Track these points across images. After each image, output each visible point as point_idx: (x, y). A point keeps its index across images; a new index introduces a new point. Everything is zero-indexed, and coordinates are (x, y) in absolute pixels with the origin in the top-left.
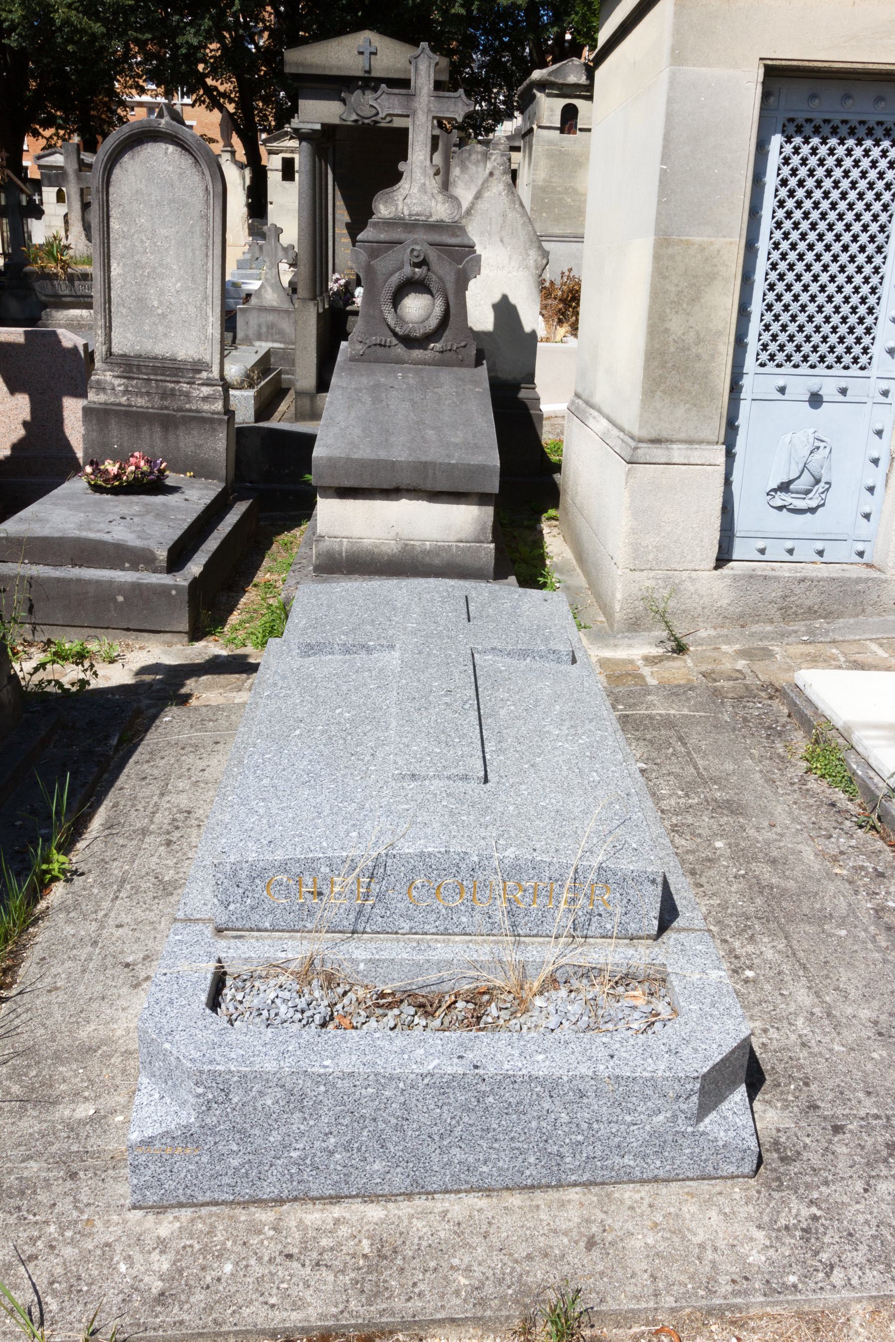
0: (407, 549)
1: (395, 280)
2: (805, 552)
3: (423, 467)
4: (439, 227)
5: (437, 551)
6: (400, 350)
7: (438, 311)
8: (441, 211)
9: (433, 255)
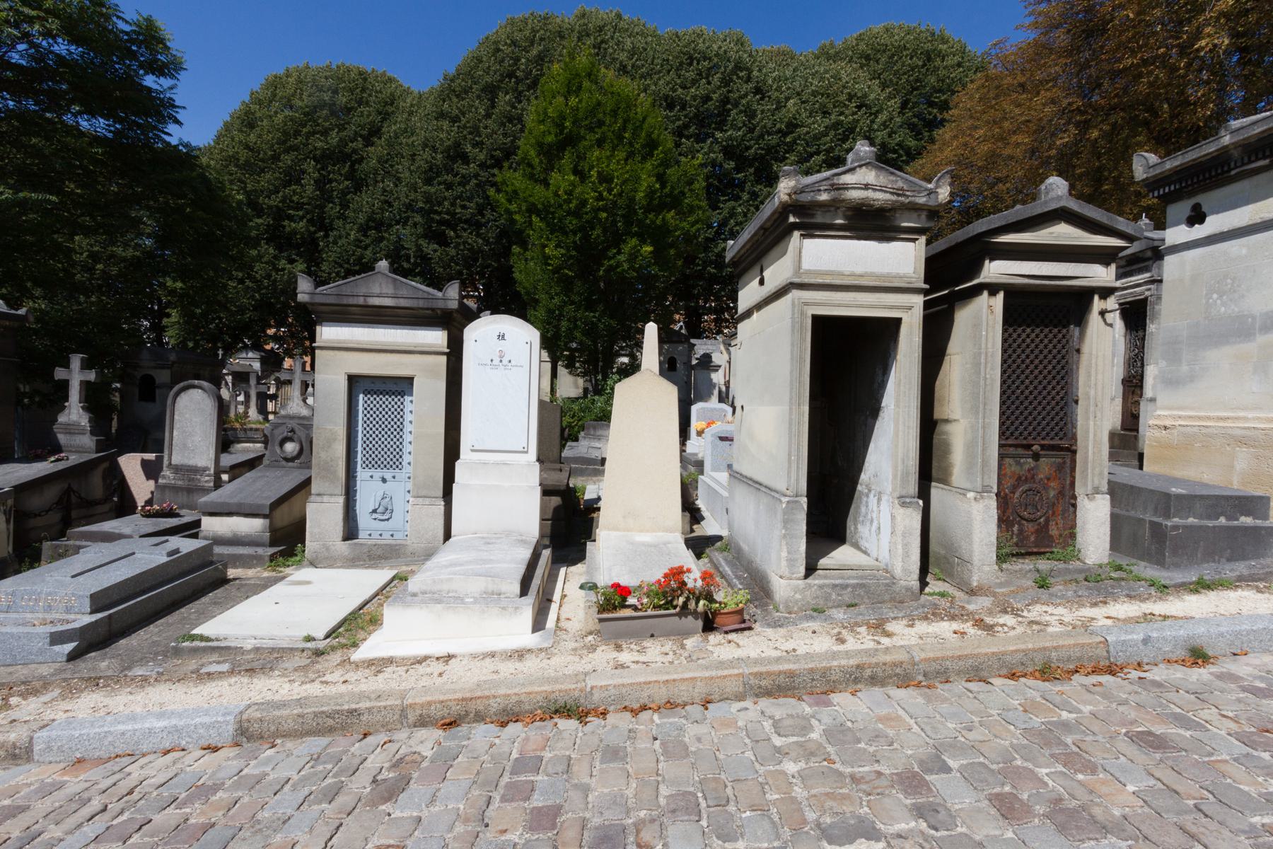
0: (235, 535)
1: (280, 437)
2: (386, 535)
3: (240, 505)
4: (304, 418)
5: (247, 536)
6: (284, 463)
7: (298, 448)
8: (305, 412)
9: (297, 428)
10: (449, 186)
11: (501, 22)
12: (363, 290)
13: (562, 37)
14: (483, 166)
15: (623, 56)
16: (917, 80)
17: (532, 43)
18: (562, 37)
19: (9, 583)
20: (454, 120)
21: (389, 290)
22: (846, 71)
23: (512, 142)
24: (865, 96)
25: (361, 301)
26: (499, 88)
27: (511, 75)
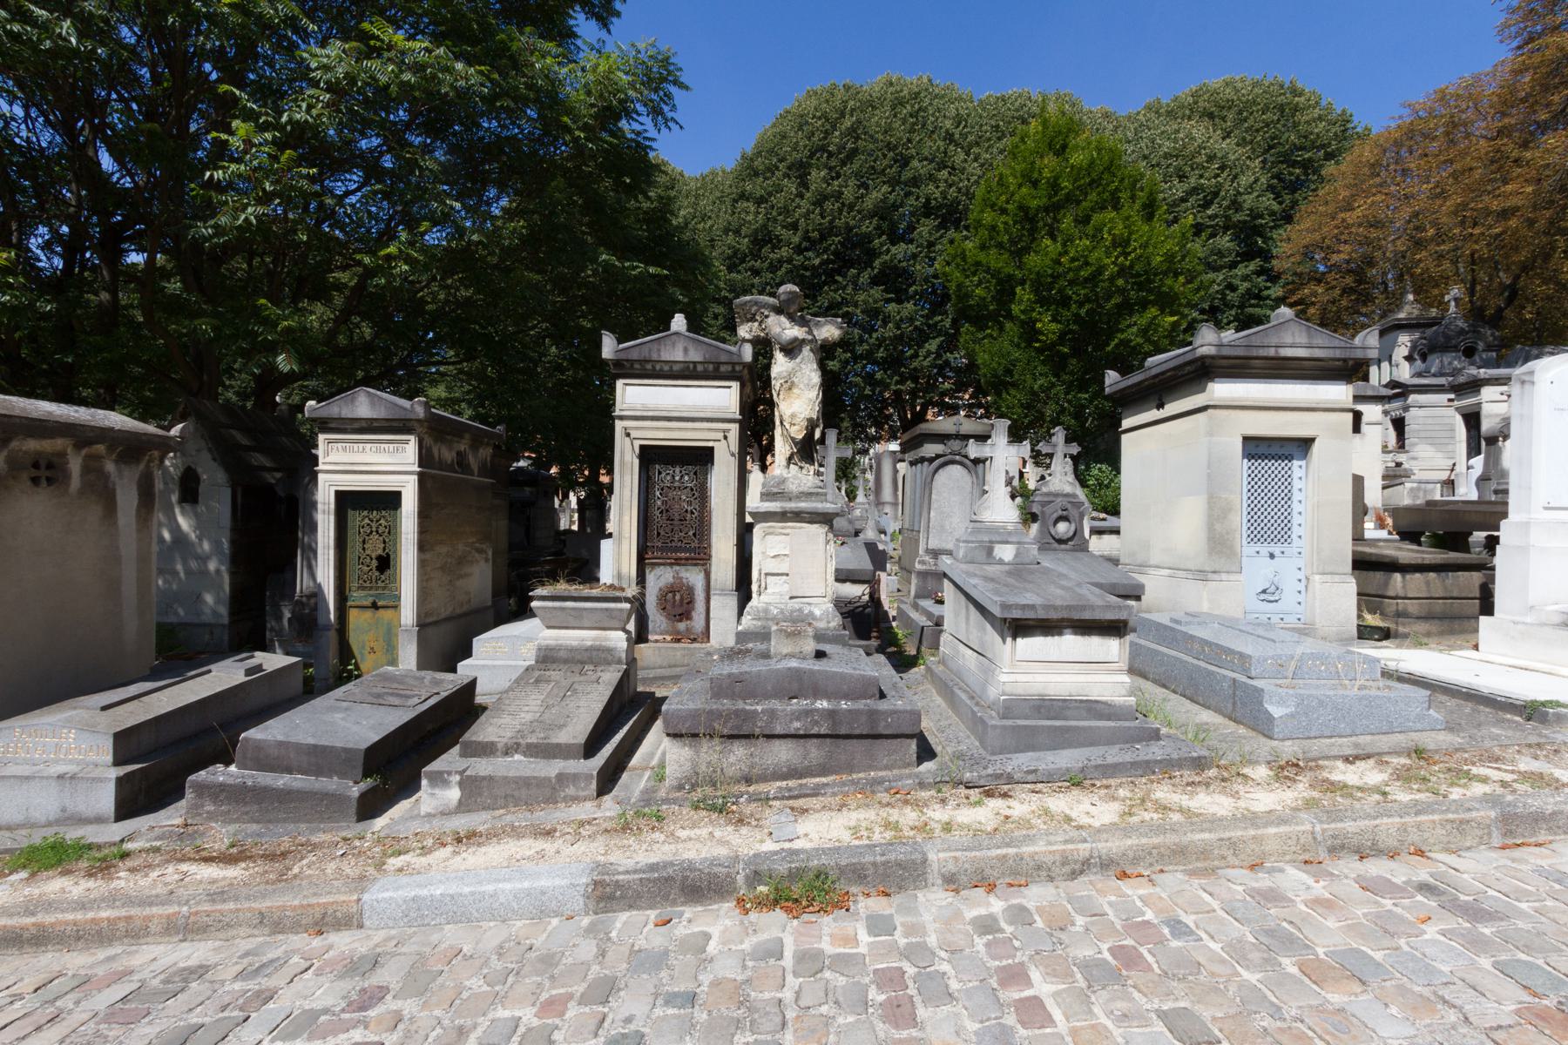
10: (756, 273)
11: (799, 95)
12: (1274, 341)
13: (874, 108)
14: (799, 250)
15: (948, 124)
16: (1273, 139)
17: (843, 115)
18: (874, 108)
19: (18, 726)
20: (760, 201)
21: (1302, 338)
22: (1199, 131)
23: (831, 222)
24: (1225, 157)
25: (1272, 352)
26: (810, 165)
27: (823, 149)
